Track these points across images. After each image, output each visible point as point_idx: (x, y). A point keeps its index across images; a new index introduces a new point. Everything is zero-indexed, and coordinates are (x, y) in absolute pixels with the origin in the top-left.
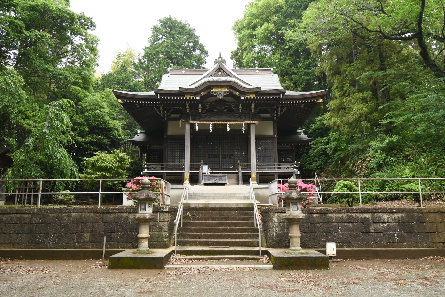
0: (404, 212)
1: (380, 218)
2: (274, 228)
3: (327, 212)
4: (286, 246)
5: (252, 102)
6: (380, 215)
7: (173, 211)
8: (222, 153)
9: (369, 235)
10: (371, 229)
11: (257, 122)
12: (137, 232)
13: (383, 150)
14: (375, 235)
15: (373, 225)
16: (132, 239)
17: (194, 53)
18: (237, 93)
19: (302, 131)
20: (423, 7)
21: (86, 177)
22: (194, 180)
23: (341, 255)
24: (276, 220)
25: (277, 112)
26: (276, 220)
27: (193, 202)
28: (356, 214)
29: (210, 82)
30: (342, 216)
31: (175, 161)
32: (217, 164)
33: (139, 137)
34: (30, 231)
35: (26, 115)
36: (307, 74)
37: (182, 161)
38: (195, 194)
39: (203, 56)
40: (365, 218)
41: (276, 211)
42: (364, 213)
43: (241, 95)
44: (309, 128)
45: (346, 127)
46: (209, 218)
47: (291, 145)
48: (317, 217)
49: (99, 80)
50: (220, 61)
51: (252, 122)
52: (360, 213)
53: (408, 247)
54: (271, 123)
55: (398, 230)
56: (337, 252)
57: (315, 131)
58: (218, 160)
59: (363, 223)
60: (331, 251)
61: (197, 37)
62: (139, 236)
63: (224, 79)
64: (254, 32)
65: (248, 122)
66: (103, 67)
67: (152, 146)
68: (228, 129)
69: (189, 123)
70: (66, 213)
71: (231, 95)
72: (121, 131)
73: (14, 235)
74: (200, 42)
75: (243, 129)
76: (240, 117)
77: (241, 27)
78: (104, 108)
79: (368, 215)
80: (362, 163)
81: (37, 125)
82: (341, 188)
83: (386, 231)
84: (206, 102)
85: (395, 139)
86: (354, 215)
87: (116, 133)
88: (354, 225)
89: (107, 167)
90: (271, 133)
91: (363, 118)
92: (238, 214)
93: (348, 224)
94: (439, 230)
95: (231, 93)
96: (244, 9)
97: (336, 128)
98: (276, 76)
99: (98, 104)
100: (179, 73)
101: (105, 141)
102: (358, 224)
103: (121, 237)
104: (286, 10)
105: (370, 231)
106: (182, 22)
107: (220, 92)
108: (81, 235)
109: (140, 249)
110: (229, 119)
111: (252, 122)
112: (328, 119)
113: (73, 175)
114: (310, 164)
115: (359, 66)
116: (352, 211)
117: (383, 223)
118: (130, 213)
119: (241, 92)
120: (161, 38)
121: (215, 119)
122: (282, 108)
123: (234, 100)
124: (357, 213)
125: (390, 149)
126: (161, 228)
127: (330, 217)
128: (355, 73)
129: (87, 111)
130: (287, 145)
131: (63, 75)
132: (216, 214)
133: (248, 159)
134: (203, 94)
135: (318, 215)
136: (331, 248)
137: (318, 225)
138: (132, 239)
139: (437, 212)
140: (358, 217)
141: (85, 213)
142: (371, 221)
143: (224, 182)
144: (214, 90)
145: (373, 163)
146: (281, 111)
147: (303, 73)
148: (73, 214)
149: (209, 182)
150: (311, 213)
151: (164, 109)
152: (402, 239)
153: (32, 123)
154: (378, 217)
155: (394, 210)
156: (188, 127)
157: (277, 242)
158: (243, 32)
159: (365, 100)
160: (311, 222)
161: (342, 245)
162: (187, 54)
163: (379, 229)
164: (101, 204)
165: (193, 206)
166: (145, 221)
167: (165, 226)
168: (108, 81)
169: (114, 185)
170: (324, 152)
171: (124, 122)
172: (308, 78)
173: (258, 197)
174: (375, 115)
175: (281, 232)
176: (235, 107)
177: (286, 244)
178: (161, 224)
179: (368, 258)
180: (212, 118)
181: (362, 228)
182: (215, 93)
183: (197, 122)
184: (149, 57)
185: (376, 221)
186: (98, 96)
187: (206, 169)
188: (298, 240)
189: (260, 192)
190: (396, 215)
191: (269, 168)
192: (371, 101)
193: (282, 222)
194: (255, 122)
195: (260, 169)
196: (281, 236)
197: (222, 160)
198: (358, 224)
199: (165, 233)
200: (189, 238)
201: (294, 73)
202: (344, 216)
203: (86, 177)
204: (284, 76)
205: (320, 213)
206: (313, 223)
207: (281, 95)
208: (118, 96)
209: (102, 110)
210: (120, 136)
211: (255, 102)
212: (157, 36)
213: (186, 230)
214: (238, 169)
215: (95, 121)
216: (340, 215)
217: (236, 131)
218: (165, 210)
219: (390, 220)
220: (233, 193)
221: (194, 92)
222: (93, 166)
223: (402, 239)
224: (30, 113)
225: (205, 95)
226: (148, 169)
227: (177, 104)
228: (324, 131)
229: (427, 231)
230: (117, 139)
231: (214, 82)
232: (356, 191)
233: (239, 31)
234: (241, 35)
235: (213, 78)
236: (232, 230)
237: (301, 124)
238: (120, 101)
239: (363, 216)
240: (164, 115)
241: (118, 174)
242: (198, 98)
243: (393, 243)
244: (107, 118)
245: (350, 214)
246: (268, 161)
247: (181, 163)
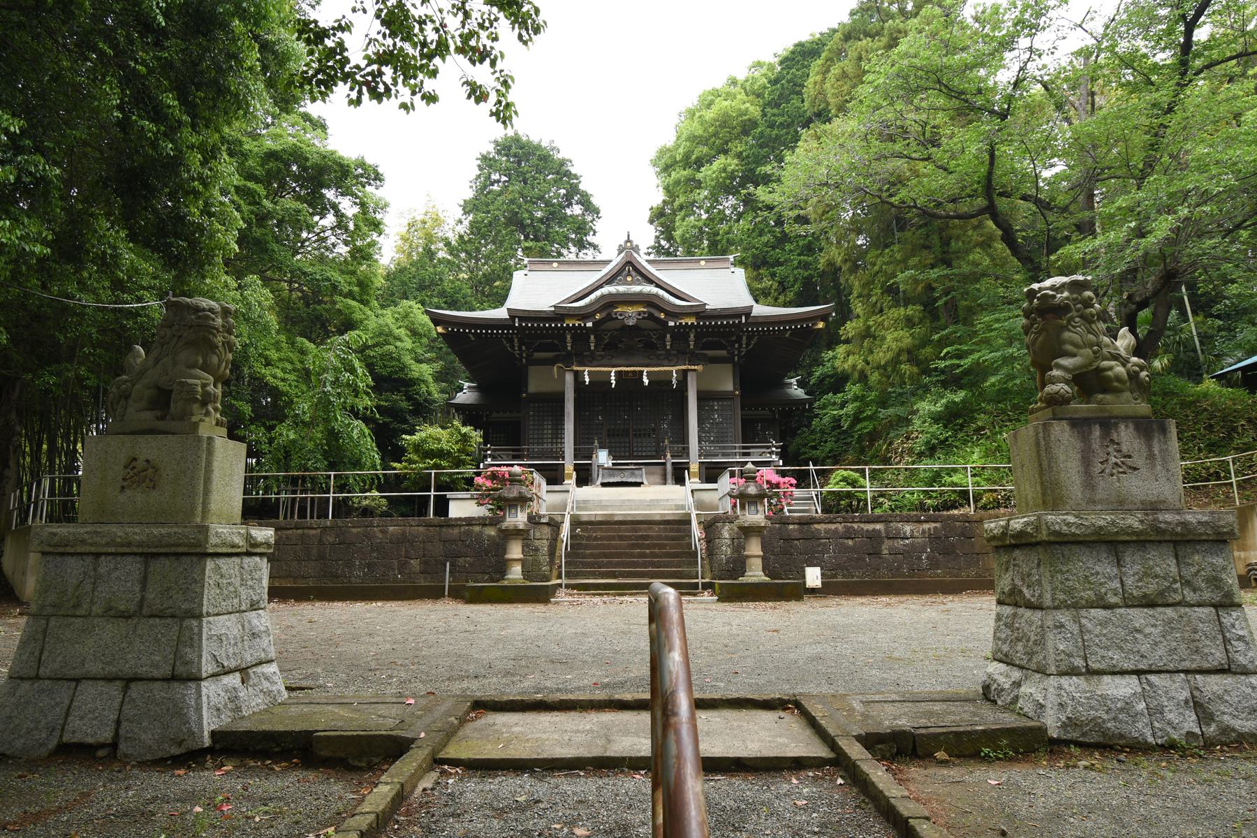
2: (724, 548)
6: (900, 525)
7: (555, 525)
8: (635, 425)
11: (699, 368)
12: (505, 551)
13: (936, 418)
17: (568, 212)
18: (662, 316)
19: (793, 380)
20: (992, 163)
21: (405, 468)
22: (584, 478)
24: (726, 535)
25: (740, 346)
26: (726, 535)
27: (585, 514)
29: (610, 295)
31: (542, 444)
33: (466, 396)
34: (321, 557)
35: (266, 358)
36: (806, 266)
38: (585, 502)
39: (589, 218)
44: (810, 374)
45: (876, 374)
47: (771, 410)
48: (794, 530)
50: (628, 247)
54: (729, 367)
57: (823, 379)
61: (576, 177)
62: (508, 556)
63: (636, 289)
64: (699, 176)
65: (684, 367)
66: (389, 252)
67: (494, 414)
68: (646, 381)
71: (651, 317)
73: (295, 563)
74: (582, 187)
75: (674, 381)
77: (669, 162)
78: (400, 340)
79: (878, 526)
80: (903, 443)
81: (287, 376)
82: (837, 483)
83: (908, 552)
85: (959, 397)
86: (856, 526)
87: (424, 389)
89: (442, 450)
90: (729, 387)
91: (904, 357)
92: (665, 530)
95: (651, 315)
96: (676, 120)
97: (856, 375)
98: (740, 273)
99: (390, 334)
100: (547, 267)
101: (404, 405)
103: (471, 565)
104: (762, 132)
106: (544, 144)
107: (631, 314)
108: (406, 563)
110: (647, 361)
112: (841, 358)
113: (374, 467)
114: (814, 448)
115: (898, 256)
118: (485, 525)
119: (667, 313)
120: (498, 181)
121: (620, 362)
122: (749, 339)
123: (657, 326)
125: (952, 417)
126: (537, 550)
128: (890, 269)
132: (627, 530)
133: (683, 438)
136: (813, 577)
143: (639, 480)
145: (919, 444)
146: (748, 344)
147: (795, 262)
149: (612, 480)
151: (521, 343)
153: (280, 374)
156: (569, 378)
158: (673, 174)
159: (909, 322)
162: (555, 215)
164: (435, 514)
165: (585, 519)
166: (516, 533)
167: (544, 545)
168: (406, 283)
169: (453, 481)
170: (837, 421)
171: (438, 366)
172: (806, 274)
173: (700, 505)
174: (928, 351)
176: (658, 339)
178: (537, 543)
180: (614, 361)
183: (587, 369)
184: (479, 229)
186: (388, 317)
187: (603, 458)
188: (759, 562)
189: (706, 497)
190: (926, 526)
191: (724, 455)
192: (920, 323)
195: (706, 456)
196: (735, 561)
199: (544, 558)
201: (778, 263)
202: (840, 527)
203: (405, 468)
204: (759, 268)
206: (788, 540)
208: (437, 320)
209: (398, 344)
210: (429, 394)
212: (489, 177)
213: (577, 555)
214: (665, 456)
216: (833, 527)
217: (660, 383)
218: (543, 520)
220: (654, 498)
221: (583, 315)
222: (417, 447)
223: (934, 564)
224: (273, 355)
225: (600, 320)
226: (494, 458)
227: (546, 334)
228: (838, 382)
230: (425, 400)
231: (618, 294)
232: (861, 487)
233: (667, 169)
234: (670, 180)
236: (653, 555)
237: (791, 366)
238: (440, 329)
239: (870, 527)
240: (521, 355)
241: (459, 463)
242: (589, 324)
244: (408, 359)
246: (722, 442)
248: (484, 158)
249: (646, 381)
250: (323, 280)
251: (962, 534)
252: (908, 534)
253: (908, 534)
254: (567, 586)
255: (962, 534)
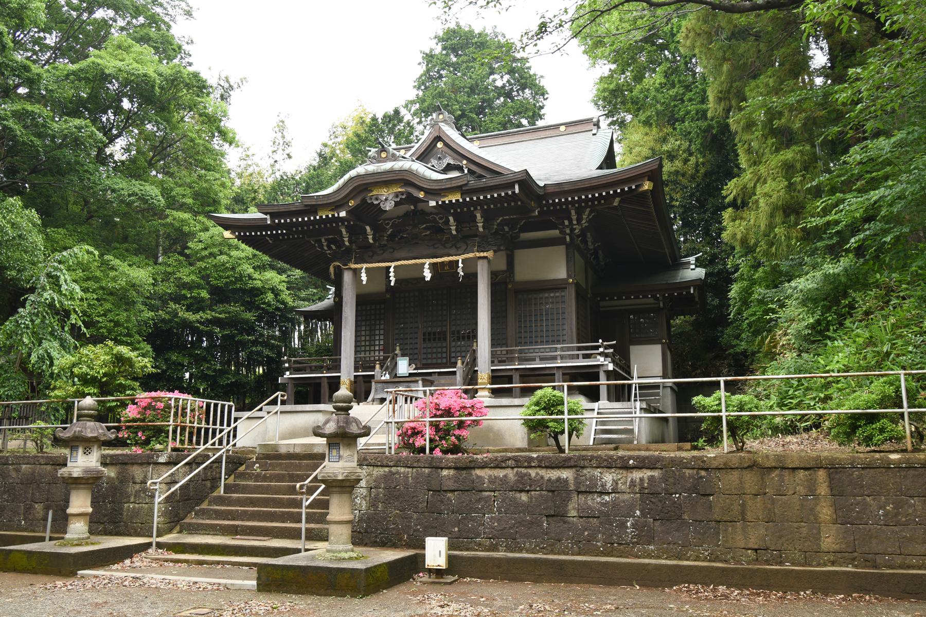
0: (658, 465)
1: (593, 479)
3: (472, 465)
4: (376, 542)
5: (476, 209)
6: (597, 472)
9: (565, 522)
10: (570, 507)
14: (580, 523)
15: (575, 497)
16: (105, 516)
18: (421, 195)
23: (456, 568)
28: (538, 470)
30: (505, 476)
32: (442, 353)
37: (370, 351)
40: (559, 479)
41: (366, 463)
42: (558, 467)
43: (430, 196)
46: (284, 475)
47: (654, 297)
49: (261, 190)
51: (478, 254)
52: (547, 467)
53: (658, 557)
54: (562, 249)
55: (638, 513)
56: (450, 559)
58: (444, 345)
59: (553, 491)
60: (435, 556)
63: (387, 166)
65: (471, 255)
68: (428, 275)
69: (350, 269)
70: (13, 464)
72: (288, 292)
76: (455, 245)
79: (566, 474)
83: (607, 515)
84: (385, 220)
86: (533, 473)
88: (531, 498)
93: (518, 495)
94: (749, 516)
95: (409, 195)
102: (541, 495)
105: (566, 512)
106: (489, 31)
109: (67, 536)
111: (478, 254)
116: (529, 463)
117: (601, 493)
119: (428, 192)
124: (540, 467)
127: (478, 477)
129: (202, 259)
130: (645, 297)
131: (137, 195)
134: (352, 203)
135: (452, 472)
136: (436, 551)
137: (449, 495)
138: (105, 516)
139: (749, 467)
140: (542, 477)
141: (40, 464)
142: (572, 487)
144: (375, 193)
146: (579, 220)
148: (24, 466)
150: (437, 468)
152: (645, 535)
154: (591, 480)
155: (631, 462)
157: (360, 532)
160: (435, 488)
161: (497, 544)
163: (589, 508)
165: (283, 450)
175: (371, 511)
177: (376, 537)
179: (537, 580)
181: (550, 504)
182: (377, 199)
183: (365, 266)
185: (583, 489)
190: (637, 475)
191: (542, 359)
193: (375, 488)
194: (485, 254)
197: (453, 344)
198: (541, 495)
200: (216, 519)
202: (511, 474)
205: (456, 468)
207: (517, 187)
211: (482, 208)
215: (221, 277)
216: (501, 473)
219: (621, 487)
229: (716, 517)
235: (367, 167)
239: (554, 474)
242: (343, 214)
243: (620, 544)
245: (524, 471)
247: (367, 354)
248: (429, 57)
249: (428, 275)
250: (130, 195)
251: (694, 489)
252: (609, 487)
253: (609, 487)
254: (159, 546)
255: (694, 489)
